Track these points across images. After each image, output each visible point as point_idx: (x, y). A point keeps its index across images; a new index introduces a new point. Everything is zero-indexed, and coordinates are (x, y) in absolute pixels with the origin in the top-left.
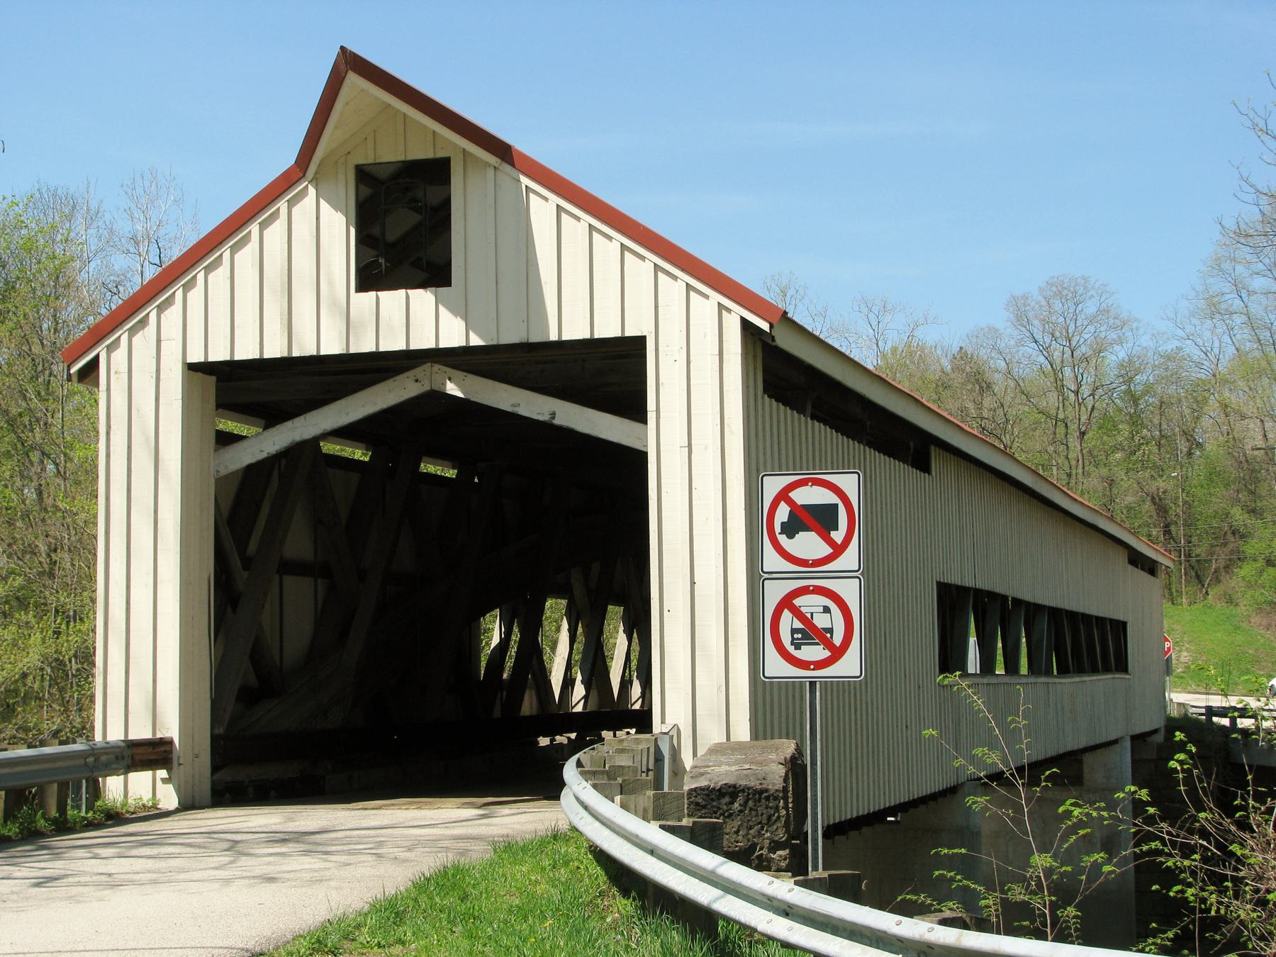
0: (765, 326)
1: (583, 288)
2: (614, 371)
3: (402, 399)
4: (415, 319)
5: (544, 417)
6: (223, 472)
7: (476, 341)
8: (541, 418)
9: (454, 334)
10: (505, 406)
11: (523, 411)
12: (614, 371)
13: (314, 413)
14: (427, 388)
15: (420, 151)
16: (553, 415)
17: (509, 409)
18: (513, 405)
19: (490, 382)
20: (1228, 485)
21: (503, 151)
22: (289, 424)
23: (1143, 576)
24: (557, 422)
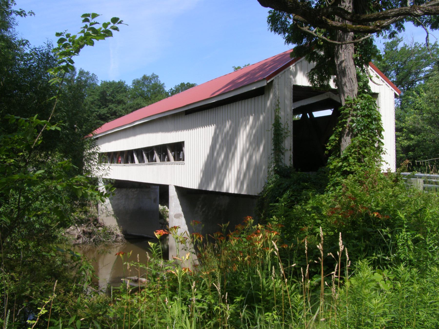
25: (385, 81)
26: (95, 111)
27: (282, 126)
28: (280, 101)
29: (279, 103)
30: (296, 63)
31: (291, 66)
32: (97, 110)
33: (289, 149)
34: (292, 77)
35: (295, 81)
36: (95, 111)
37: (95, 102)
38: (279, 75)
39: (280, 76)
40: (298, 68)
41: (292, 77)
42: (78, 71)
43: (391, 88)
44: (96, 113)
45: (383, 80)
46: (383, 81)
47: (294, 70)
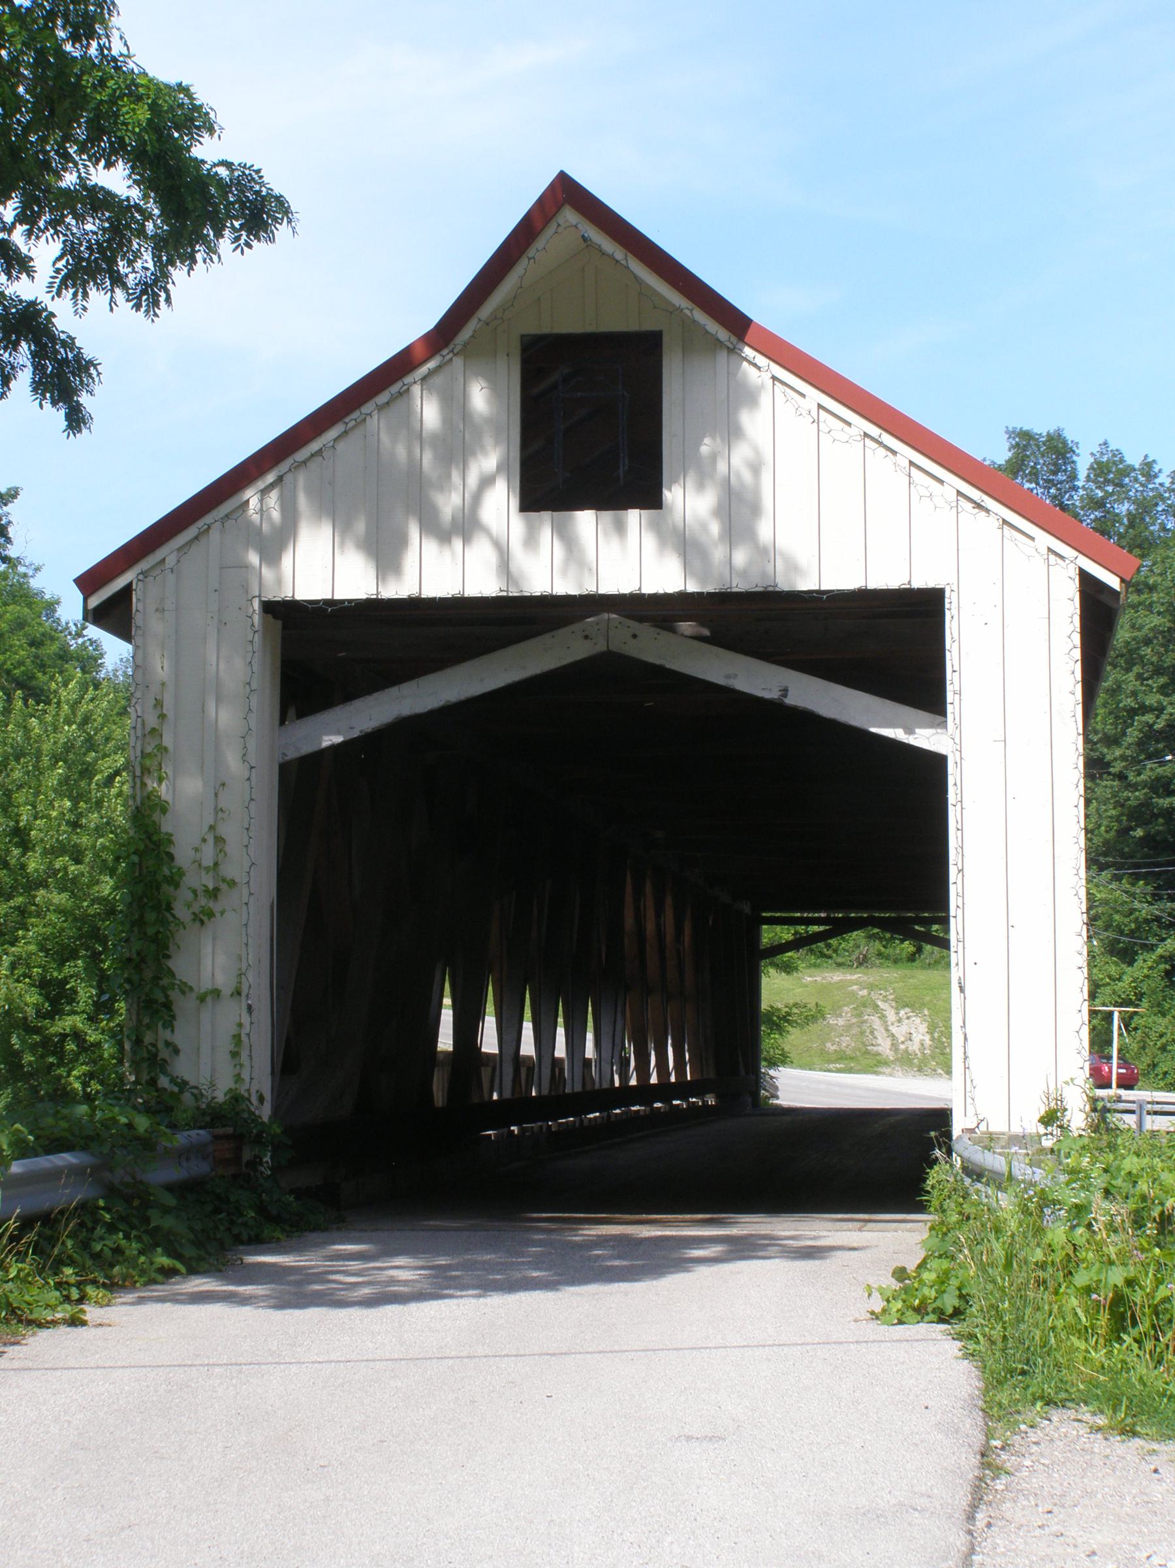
0: (1113, 582)
1: (802, 496)
2: (898, 640)
3: (564, 662)
4: (618, 557)
5: (772, 694)
6: (292, 754)
7: (692, 587)
8: (767, 695)
9: (664, 576)
10: (769, 693)
11: (743, 685)
12: (898, 640)
13: (431, 677)
14: (601, 647)
15: (616, 319)
16: (785, 692)
17: (721, 681)
18: (728, 677)
19: (783, 669)
20: (1127, 1198)
21: (737, 324)
22: (394, 691)
23: (984, 514)
24: (790, 701)
25: (989, 503)
26: (1143, 709)
27: (183, 853)
28: (168, 708)
29: (162, 716)
30: (284, 466)
31: (251, 496)
32: (1152, 700)
33: (227, 991)
34: (254, 558)
35: (279, 581)
36: (1143, 709)
37: (1147, 651)
38: (167, 552)
39: (171, 561)
40: (302, 501)
41: (254, 558)
42: (1083, 464)
43: (1045, 540)
44: (1149, 718)
45: (975, 494)
46: (978, 506)
47: (276, 515)
